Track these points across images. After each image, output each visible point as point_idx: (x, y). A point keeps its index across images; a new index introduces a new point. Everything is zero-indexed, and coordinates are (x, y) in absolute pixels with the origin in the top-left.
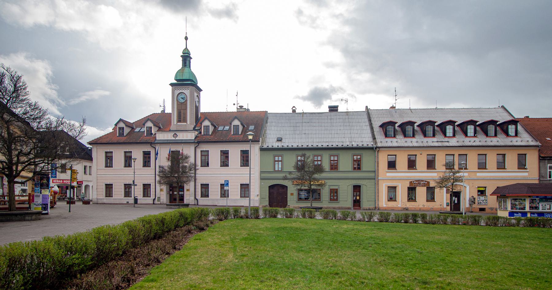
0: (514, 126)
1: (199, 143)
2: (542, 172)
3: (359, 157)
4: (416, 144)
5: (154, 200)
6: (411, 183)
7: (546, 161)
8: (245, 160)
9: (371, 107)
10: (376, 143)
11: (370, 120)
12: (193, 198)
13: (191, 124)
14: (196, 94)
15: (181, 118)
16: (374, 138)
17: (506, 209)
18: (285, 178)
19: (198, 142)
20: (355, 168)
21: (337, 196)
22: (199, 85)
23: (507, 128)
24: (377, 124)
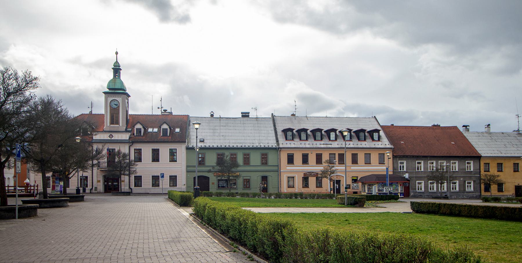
0: (377, 134)
1: (133, 143)
2: (395, 166)
4: (308, 146)
5: (91, 189)
6: (304, 174)
9: (275, 114)
10: (278, 144)
11: (275, 126)
12: (128, 188)
13: (122, 126)
14: (126, 101)
15: (114, 120)
16: (277, 141)
17: (365, 191)
18: (209, 171)
19: (132, 141)
20: (263, 164)
22: (128, 91)
23: (373, 135)
24: (280, 129)
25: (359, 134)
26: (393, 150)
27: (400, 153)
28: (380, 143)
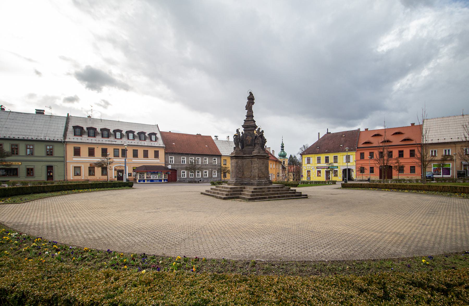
2: (166, 160)
3: (51, 147)
4: (146, 145)
6: (91, 164)
21: (33, 173)
25: (141, 135)
26: (166, 149)
27: (170, 151)
28: (156, 143)
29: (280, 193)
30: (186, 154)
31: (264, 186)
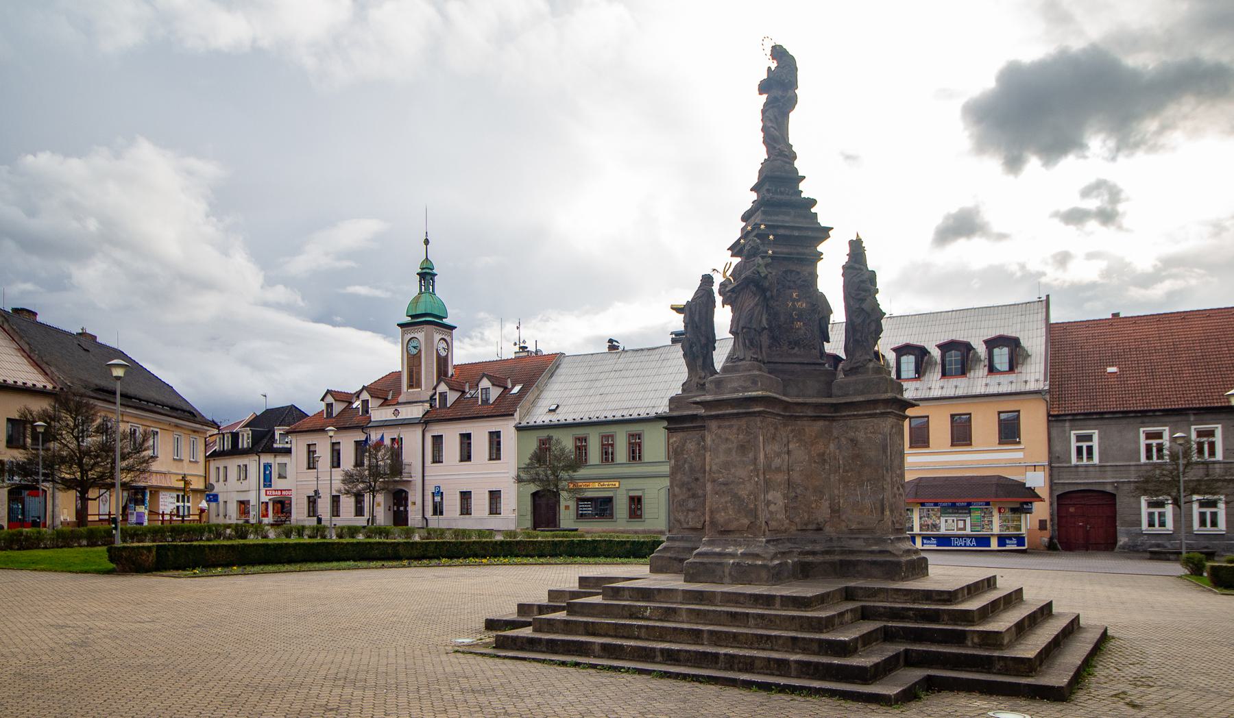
2: (1058, 448)
7: (1067, 424)
8: (495, 451)
19: (426, 421)
27: (1079, 407)
29: (717, 638)
30: (1168, 413)
31: (735, 581)
